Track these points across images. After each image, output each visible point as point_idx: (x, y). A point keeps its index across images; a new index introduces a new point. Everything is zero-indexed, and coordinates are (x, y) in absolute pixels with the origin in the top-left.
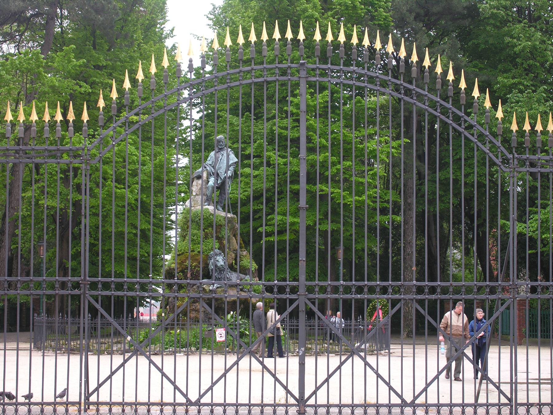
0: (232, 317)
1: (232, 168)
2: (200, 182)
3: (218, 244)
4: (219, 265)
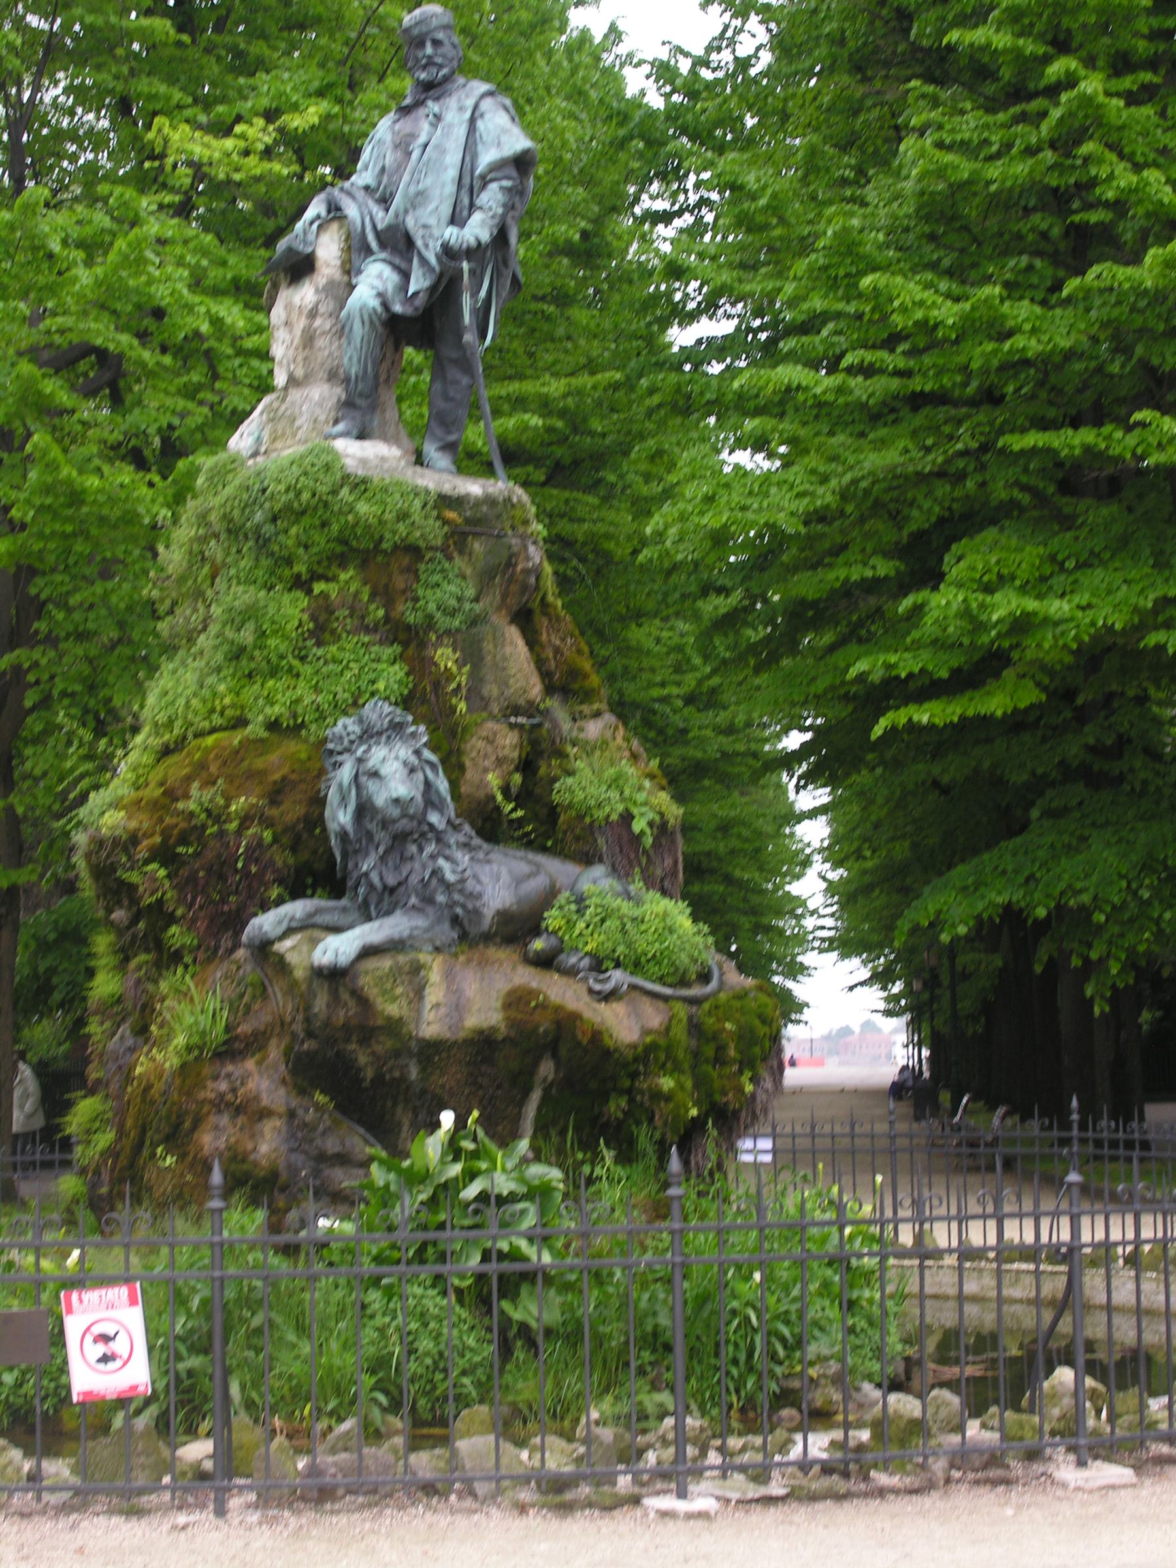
0: (453, 1150)
1: (492, 197)
2: (306, 294)
3: (397, 672)
4: (380, 800)
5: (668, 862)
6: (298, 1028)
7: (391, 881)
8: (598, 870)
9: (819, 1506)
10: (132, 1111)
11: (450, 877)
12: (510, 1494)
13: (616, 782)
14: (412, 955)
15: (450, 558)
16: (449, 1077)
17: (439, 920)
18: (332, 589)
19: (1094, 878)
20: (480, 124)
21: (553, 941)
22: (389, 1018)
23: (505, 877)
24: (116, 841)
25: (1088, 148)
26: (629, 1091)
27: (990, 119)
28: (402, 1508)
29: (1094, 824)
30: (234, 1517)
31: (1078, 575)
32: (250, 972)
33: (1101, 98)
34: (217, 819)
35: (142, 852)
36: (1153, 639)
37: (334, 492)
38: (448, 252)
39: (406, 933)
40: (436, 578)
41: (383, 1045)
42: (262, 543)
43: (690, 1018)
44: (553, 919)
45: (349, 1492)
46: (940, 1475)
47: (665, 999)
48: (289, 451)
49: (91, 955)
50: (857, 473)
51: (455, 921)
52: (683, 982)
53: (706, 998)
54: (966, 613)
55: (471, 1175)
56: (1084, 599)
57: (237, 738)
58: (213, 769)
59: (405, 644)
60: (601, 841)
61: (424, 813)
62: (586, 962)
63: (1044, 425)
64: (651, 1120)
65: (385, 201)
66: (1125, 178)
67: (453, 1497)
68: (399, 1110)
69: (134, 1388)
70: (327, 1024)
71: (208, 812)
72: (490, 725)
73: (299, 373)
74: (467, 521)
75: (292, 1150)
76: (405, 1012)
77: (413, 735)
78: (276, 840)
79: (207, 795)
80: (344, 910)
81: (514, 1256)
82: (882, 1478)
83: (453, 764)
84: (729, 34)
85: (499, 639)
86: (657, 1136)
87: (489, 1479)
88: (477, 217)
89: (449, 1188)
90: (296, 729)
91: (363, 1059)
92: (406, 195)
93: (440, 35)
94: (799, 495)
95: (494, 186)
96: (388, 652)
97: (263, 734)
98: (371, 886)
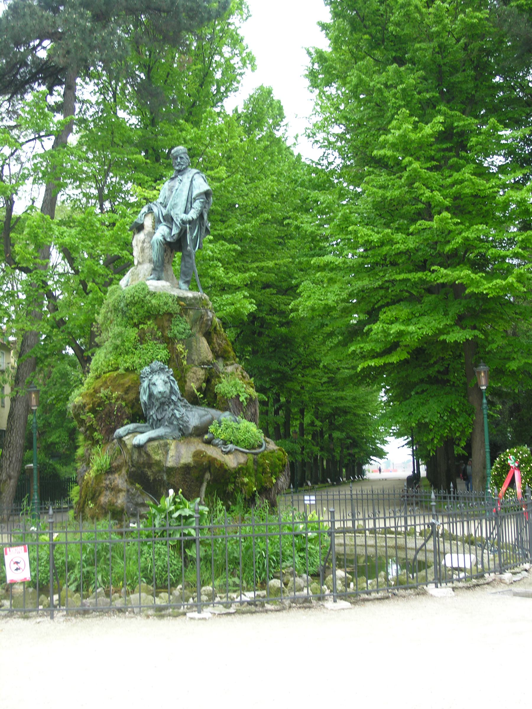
1: (197, 205)
2: (141, 236)
3: (165, 352)
5: (253, 410)
6: (130, 464)
7: (159, 417)
8: (227, 413)
9: (244, 616)
10: (83, 490)
11: (178, 416)
12: (146, 612)
13: (235, 386)
14: (166, 441)
15: (182, 316)
16: (177, 479)
17: (175, 430)
18: (145, 327)
19: (430, 414)
20: (194, 182)
21: (211, 435)
22: (156, 460)
23: (197, 415)
24: (80, 406)
25: (416, 184)
26: (234, 482)
27: (389, 178)
28: (110, 616)
29: (431, 396)
30: (56, 619)
31: (420, 318)
32: (117, 447)
33: (419, 170)
34: (109, 399)
35: (87, 410)
36: (442, 338)
37: (145, 297)
38: (184, 222)
39: (163, 434)
40: (177, 323)
41: (155, 469)
42: (124, 313)
43: (254, 459)
44: (212, 429)
45: (94, 611)
46: (287, 605)
47: (246, 453)
48: (135, 283)
49: (78, 442)
50: (354, 288)
51: (180, 430)
52: (253, 448)
53: (260, 453)
54: (384, 331)
55: (177, 509)
56: (420, 326)
57: (115, 374)
58: (108, 383)
59: (168, 344)
60: (230, 404)
61: (170, 396)
62: (221, 442)
63: (410, 272)
64: (241, 491)
65: (165, 207)
66: (428, 193)
67: (127, 613)
68: (162, 489)
69: (25, 579)
70: (137, 462)
71: (106, 397)
72: (195, 368)
73: (141, 260)
74: (187, 305)
75: (128, 502)
76: (162, 459)
77: (167, 372)
78: (126, 405)
79: (106, 391)
80: (146, 427)
81: (189, 534)
82: (268, 606)
83: (182, 380)
84: (326, 155)
85: (198, 341)
86: (243, 496)
87: (137, 607)
88: (193, 210)
89: (171, 513)
90: (134, 371)
91: (149, 473)
92: (171, 205)
93: (183, 156)
94: (336, 295)
95: (198, 201)
96: (162, 346)
97: (123, 372)
98: (154, 419)
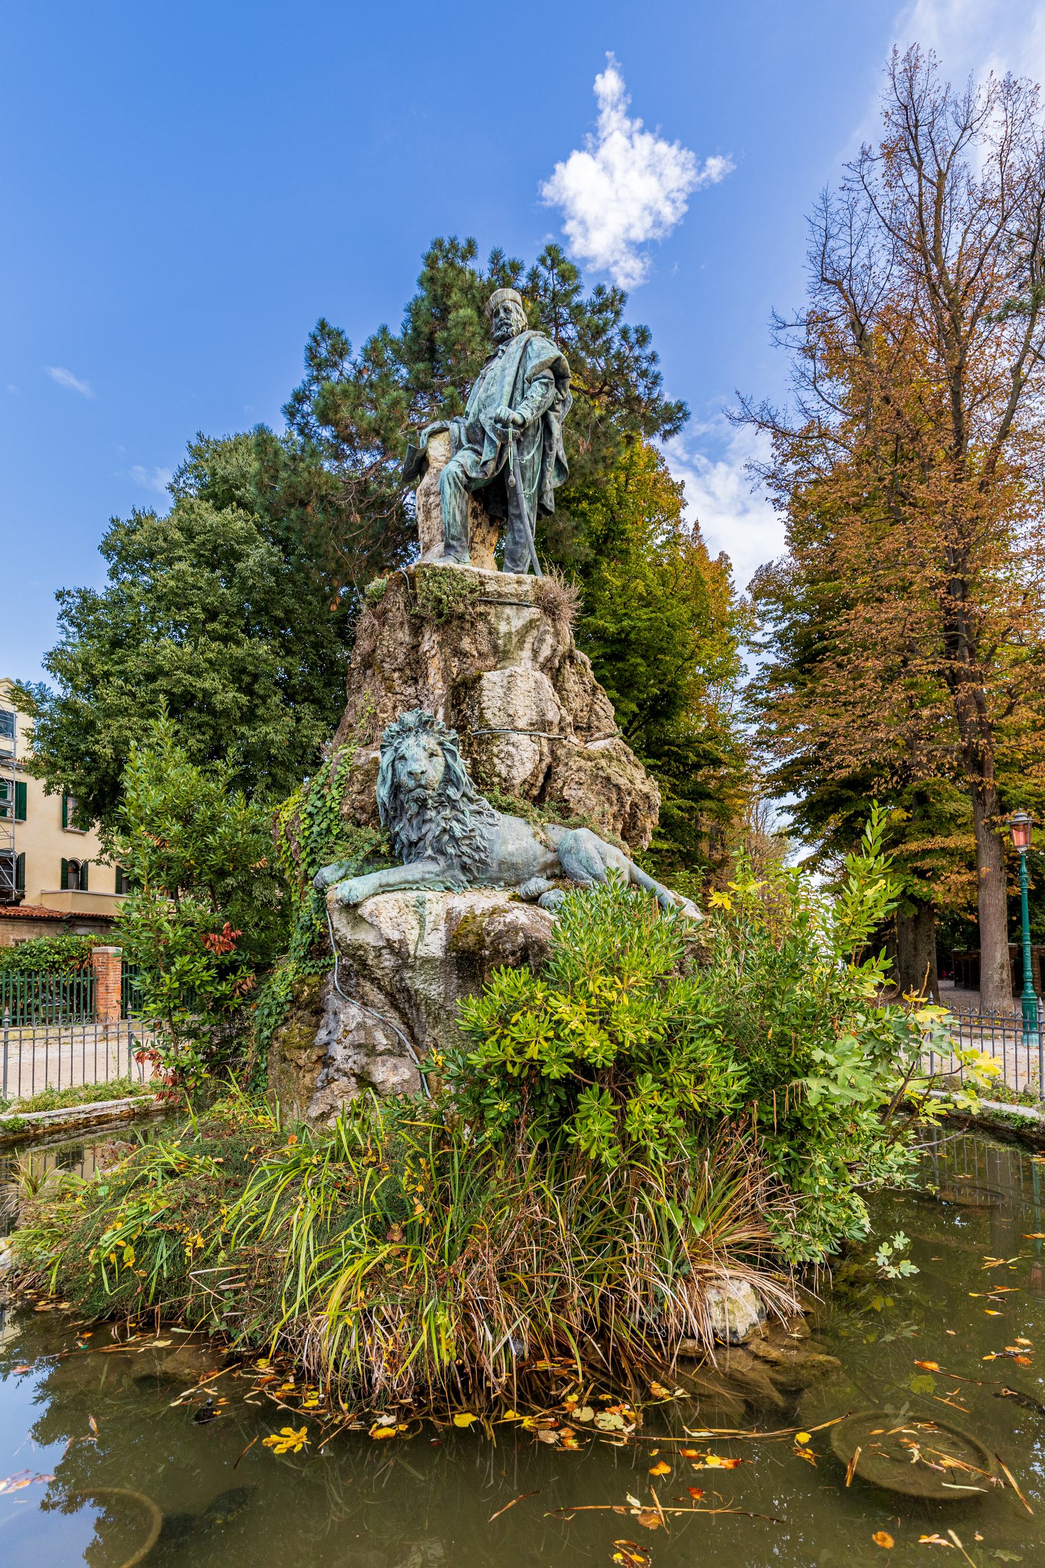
7: (414, 837)
11: (458, 833)
20: (529, 349)
